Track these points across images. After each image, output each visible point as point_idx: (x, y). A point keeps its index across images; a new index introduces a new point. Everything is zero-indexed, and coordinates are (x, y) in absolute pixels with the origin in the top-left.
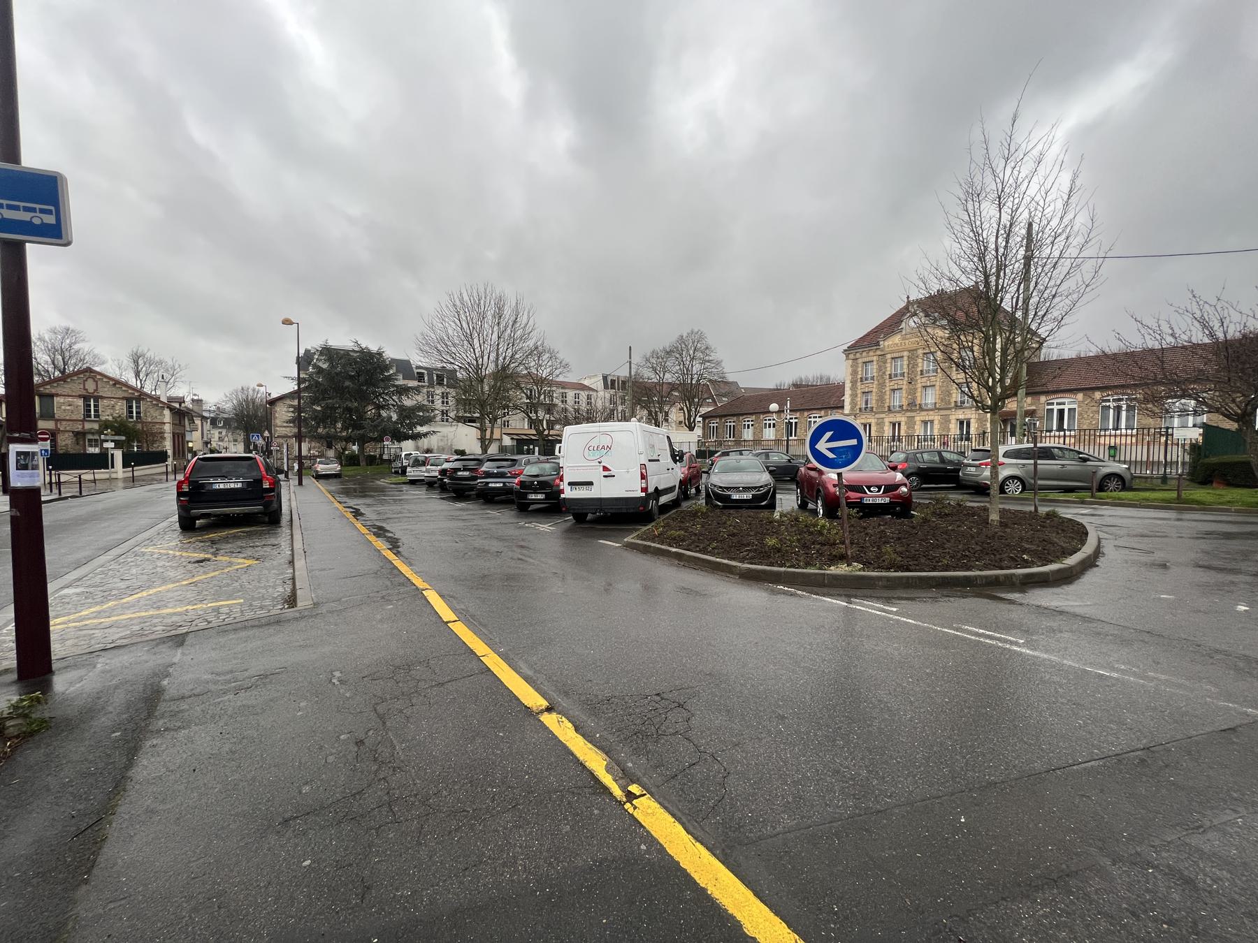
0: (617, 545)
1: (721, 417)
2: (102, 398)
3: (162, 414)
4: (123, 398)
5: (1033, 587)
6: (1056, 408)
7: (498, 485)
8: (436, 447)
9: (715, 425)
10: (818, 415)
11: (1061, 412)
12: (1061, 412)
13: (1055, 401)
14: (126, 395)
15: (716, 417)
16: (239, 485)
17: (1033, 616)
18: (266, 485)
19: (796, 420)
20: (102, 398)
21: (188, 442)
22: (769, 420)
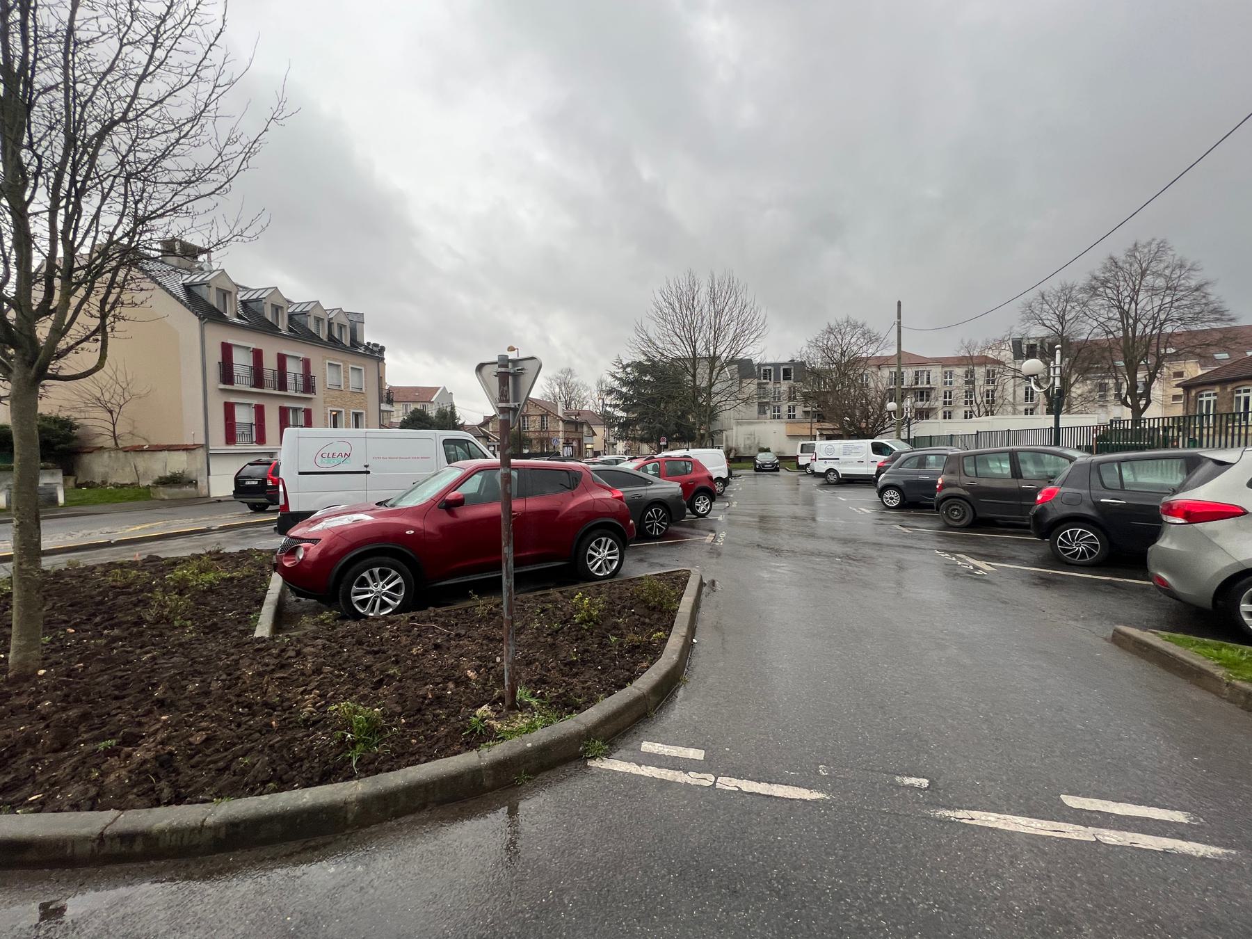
0: (61, 446)
1: (1223, 383)
2: (530, 415)
3: (558, 425)
4: (741, 382)
5: (347, 548)
6: (1243, 395)
7: (253, 483)
8: (742, 446)
9: (1212, 398)
10: (1212, 392)
11: (1208, 402)
12: (1208, 402)
13: (1242, 389)
14: (540, 413)
15: (1213, 384)
16: (256, 483)
17: (704, 838)
18: (270, 483)
19: (1215, 398)
20: (530, 415)
21: (586, 444)
22: (1207, 395)
